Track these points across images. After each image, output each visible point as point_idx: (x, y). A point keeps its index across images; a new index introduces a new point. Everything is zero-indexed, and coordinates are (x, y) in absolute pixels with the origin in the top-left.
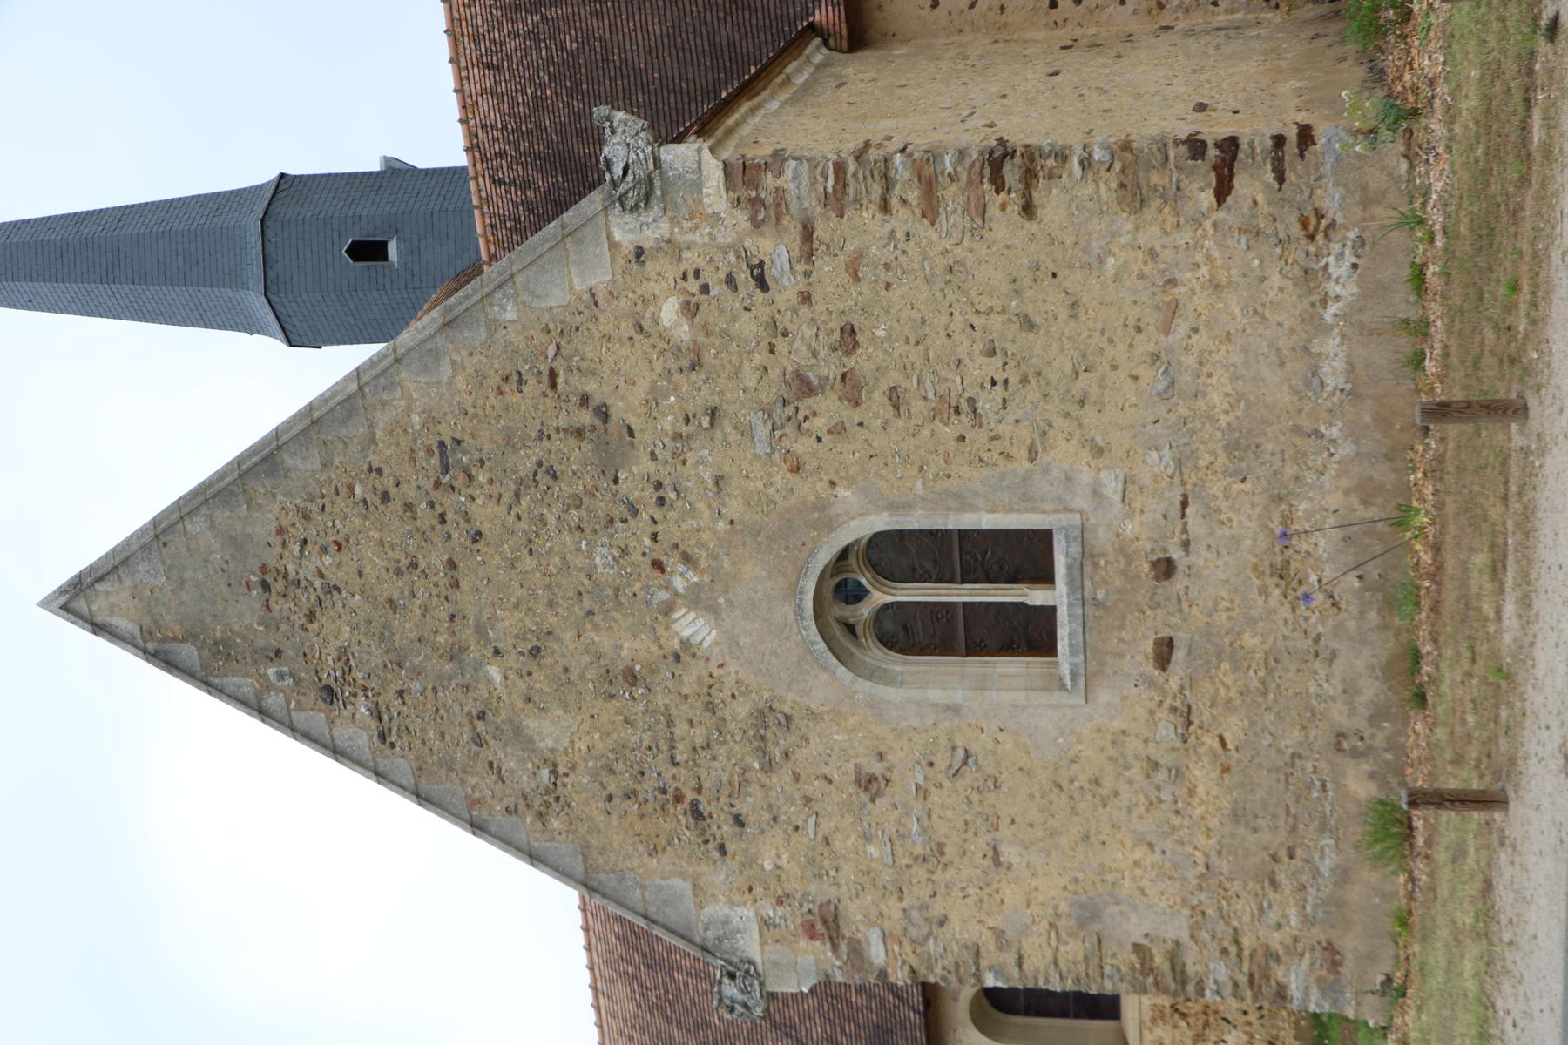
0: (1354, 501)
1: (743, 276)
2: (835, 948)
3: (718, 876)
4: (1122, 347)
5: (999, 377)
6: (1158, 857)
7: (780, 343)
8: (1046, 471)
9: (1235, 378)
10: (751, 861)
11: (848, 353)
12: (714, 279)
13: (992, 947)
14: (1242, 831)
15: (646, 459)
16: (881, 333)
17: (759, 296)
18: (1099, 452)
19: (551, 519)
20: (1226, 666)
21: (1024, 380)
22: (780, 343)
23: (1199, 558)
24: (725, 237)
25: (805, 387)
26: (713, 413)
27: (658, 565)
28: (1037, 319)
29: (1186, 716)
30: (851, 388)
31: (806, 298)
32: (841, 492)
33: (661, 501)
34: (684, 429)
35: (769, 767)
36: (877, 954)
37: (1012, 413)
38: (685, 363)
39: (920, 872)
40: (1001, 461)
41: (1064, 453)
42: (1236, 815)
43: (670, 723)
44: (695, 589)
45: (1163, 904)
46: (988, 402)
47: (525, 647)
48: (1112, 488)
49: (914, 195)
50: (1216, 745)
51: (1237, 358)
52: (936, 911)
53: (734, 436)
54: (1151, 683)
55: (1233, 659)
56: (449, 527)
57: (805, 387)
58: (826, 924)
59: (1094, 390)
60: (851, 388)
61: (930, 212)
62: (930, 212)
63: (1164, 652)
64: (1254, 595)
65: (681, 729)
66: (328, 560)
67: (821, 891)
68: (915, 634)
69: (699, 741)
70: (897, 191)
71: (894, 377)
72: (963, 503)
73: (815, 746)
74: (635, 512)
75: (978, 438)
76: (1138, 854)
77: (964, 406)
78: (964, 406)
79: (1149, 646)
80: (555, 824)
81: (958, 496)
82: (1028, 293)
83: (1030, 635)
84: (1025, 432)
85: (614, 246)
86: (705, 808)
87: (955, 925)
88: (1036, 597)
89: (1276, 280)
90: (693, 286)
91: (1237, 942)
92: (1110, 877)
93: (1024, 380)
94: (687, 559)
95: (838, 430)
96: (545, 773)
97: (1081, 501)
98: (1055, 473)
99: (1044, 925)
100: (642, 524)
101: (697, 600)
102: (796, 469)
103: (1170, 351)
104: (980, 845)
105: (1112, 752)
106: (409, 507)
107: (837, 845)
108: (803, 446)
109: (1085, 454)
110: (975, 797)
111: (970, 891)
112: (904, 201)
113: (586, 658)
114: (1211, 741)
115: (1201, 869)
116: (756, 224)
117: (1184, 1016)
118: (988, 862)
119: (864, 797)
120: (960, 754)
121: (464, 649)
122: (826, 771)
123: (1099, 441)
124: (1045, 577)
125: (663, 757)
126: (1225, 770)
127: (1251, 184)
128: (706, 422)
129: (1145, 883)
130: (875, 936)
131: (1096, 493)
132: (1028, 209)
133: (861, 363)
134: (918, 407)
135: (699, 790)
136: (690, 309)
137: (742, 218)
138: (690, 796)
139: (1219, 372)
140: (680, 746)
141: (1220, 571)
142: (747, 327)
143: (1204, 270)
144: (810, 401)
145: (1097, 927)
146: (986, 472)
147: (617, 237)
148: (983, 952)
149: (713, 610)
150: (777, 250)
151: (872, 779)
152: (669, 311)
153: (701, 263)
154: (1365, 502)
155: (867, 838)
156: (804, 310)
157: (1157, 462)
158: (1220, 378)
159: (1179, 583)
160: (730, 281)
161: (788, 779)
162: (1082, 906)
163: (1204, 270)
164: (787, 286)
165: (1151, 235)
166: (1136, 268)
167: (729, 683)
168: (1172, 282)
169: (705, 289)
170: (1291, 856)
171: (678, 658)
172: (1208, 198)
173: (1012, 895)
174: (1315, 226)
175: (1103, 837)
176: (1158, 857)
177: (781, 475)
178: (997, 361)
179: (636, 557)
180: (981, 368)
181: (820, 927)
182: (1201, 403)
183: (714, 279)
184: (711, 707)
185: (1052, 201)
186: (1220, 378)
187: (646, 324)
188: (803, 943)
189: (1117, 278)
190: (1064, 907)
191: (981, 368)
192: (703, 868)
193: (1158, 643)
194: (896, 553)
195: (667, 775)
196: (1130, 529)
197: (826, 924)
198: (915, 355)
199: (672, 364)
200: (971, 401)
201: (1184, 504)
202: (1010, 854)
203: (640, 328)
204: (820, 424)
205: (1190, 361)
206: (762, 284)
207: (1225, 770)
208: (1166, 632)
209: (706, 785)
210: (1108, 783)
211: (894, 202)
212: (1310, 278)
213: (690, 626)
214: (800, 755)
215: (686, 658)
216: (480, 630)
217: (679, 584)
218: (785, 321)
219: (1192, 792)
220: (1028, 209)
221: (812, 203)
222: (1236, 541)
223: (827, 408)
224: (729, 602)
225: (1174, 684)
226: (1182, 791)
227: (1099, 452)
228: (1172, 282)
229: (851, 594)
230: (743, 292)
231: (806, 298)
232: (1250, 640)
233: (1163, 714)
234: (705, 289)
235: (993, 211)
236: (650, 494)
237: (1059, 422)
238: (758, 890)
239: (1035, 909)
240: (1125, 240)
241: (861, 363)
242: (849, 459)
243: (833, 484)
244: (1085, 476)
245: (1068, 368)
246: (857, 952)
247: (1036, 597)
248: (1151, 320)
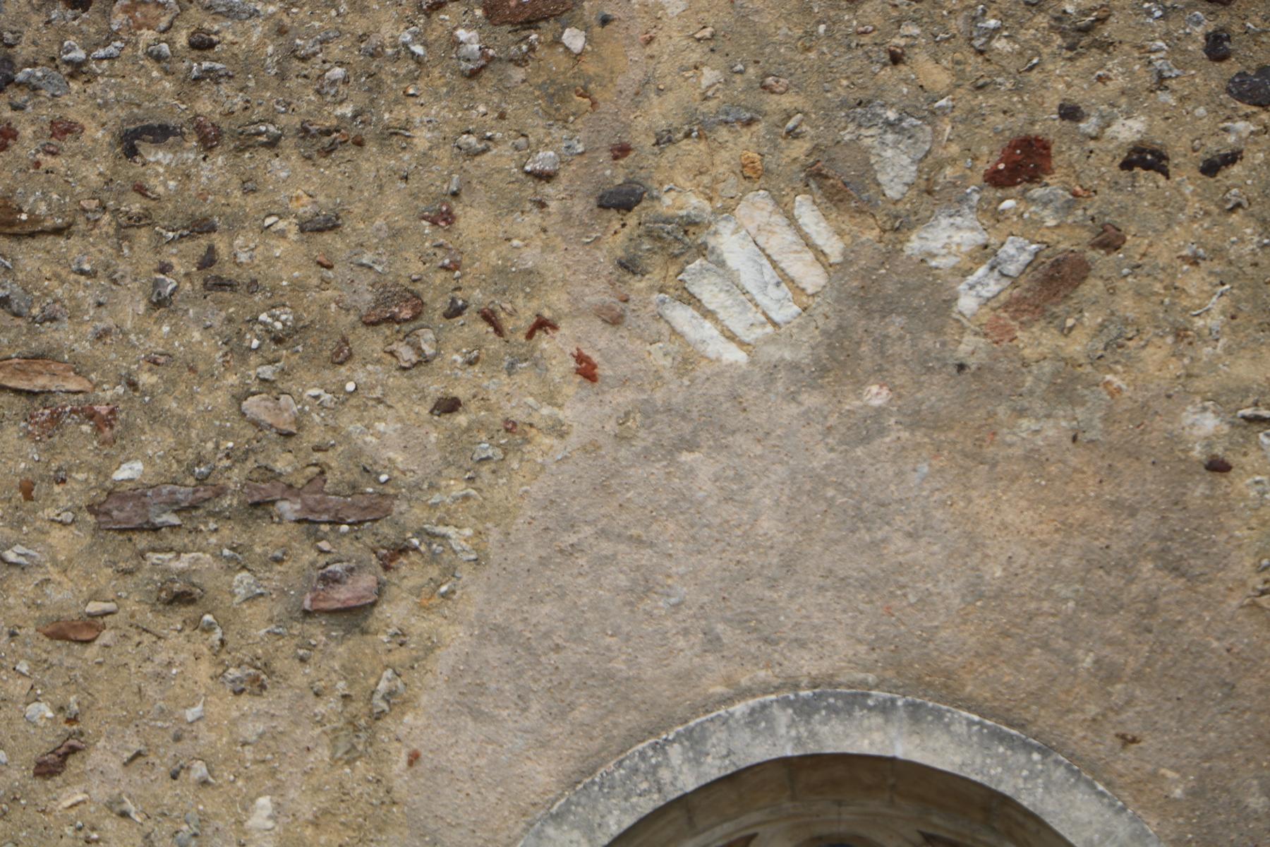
27: (1024, 163)
35: (121, 520)
43: (323, 142)
44: (929, 299)
65: (294, 181)
69: (239, 250)
94: (1056, 279)
122: (103, 756)
140: (214, 170)
149: (835, 361)
167: (513, 395)
171: (621, 200)
195: (74, 102)
214: (180, 647)
215: (618, 235)
217: (947, 238)
224: (867, 428)
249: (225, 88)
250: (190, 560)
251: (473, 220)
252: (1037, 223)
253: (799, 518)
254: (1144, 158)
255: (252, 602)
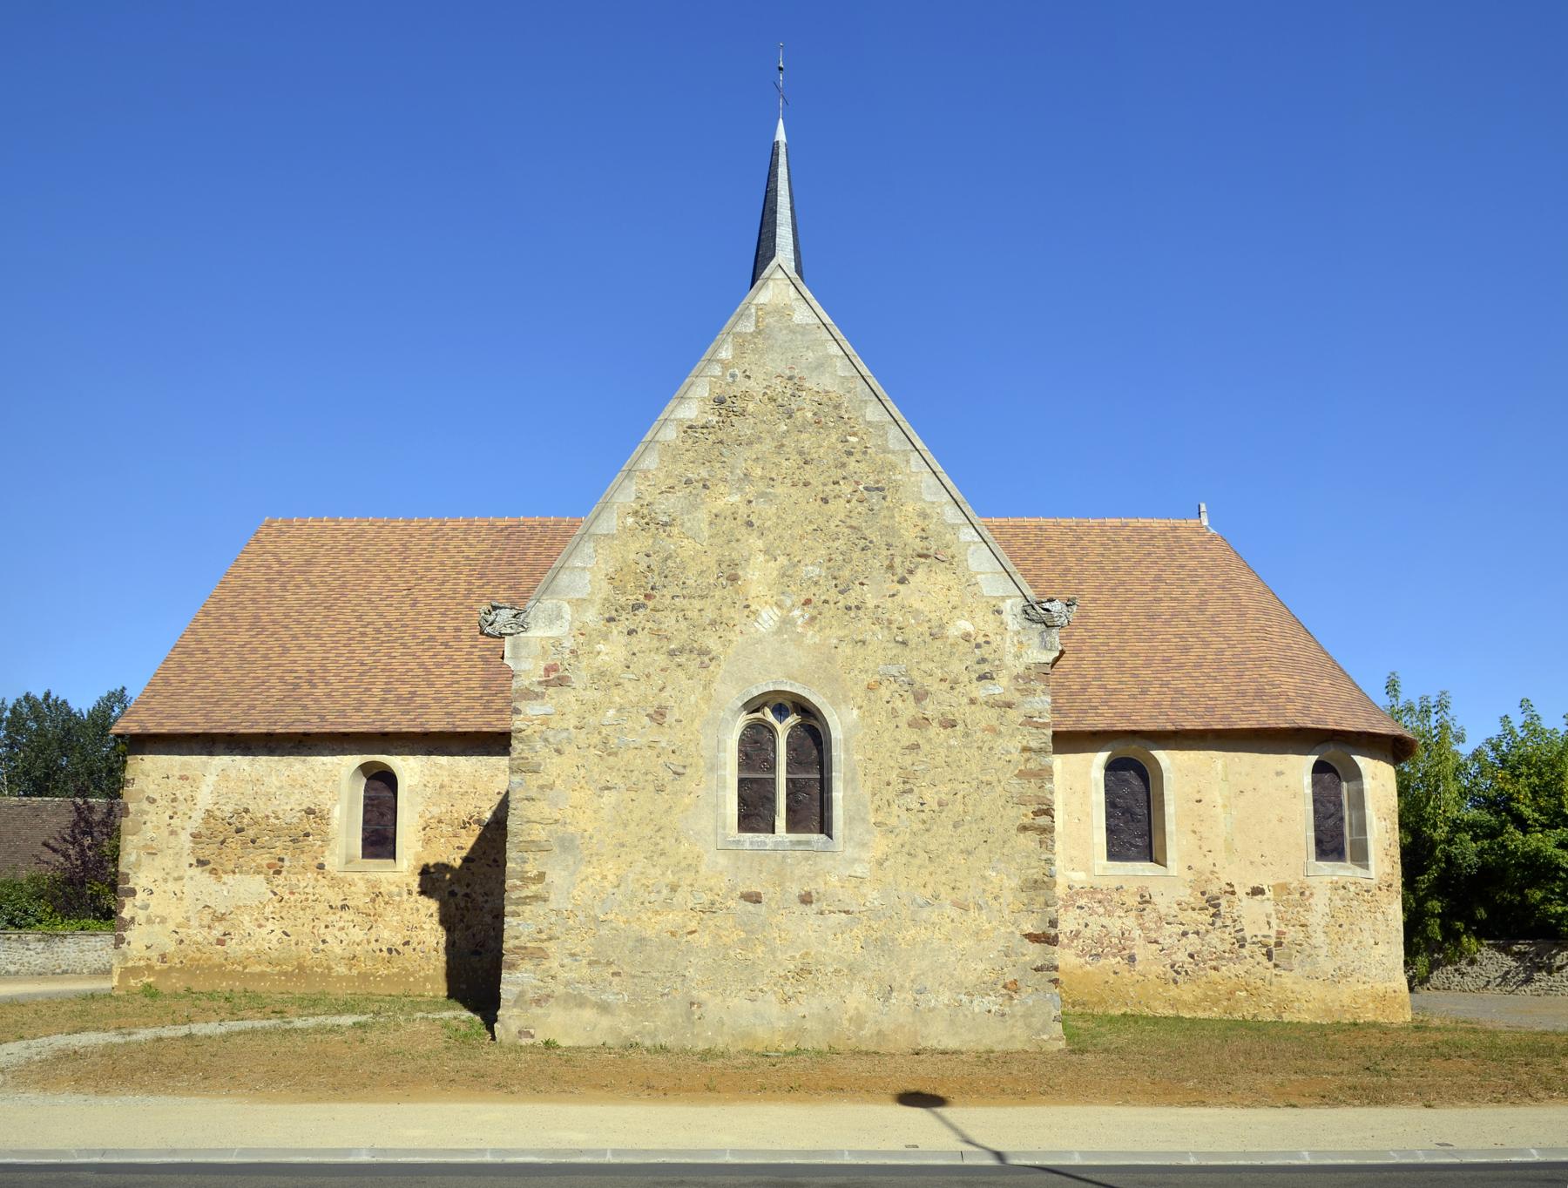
0: (852, 1012)
1: (986, 668)
2: (540, 683)
3: (591, 616)
4: (943, 879)
5: (925, 808)
6: (611, 890)
7: (946, 686)
8: (868, 832)
9: (925, 943)
10: (605, 637)
11: (941, 723)
12: (985, 651)
13: (541, 782)
14: (630, 944)
15: (875, 602)
16: (952, 742)
17: (974, 676)
18: (880, 864)
19: (836, 544)
20: (743, 935)
21: (924, 822)
22: (946, 686)
23: (813, 921)
24: (1009, 660)
25: (920, 697)
26: (904, 643)
27: (807, 602)
28: (960, 830)
29: (711, 909)
30: (920, 723)
31: (972, 702)
32: (855, 712)
33: (848, 608)
34: (894, 626)
35: (672, 653)
36: (531, 709)
37: (904, 815)
38: (935, 630)
39: (596, 739)
40: (874, 806)
41: (880, 845)
42: (642, 941)
43: (702, 597)
44: (793, 622)
45: (575, 893)
46: (911, 801)
47: (753, 518)
48: (859, 870)
49: (1032, 765)
50: (690, 929)
51: (935, 945)
52: (567, 749)
53: (890, 654)
54: (733, 890)
55: (746, 940)
56: (831, 486)
57: (920, 697)
58: (556, 679)
59: (917, 862)
60: (920, 723)
61: (1021, 774)
62: (1021, 774)
63: (754, 898)
64: (790, 953)
65: (698, 604)
66: (809, 415)
67: (580, 677)
68: (755, 746)
69: (689, 614)
70: (1033, 755)
71: (926, 747)
72: (850, 782)
73: (685, 683)
74: (841, 592)
75: (889, 793)
76: (611, 877)
77: (908, 786)
78: (908, 786)
79: (755, 889)
80: (630, 520)
81: (853, 780)
82: (974, 827)
83: (754, 813)
84: (893, 821)
85: (1003, 599)
86: (641, 612)
87: (557, 759)
88: (781, 822)
89: (981, 967)
90: (981, 640)
91: (550, 939)
92: (594, 859)
93: (924, 822)
94: (813, 619)
95: (894, 713)
96: (665, 519)
97: (850, 852)
98: (867, 837)
99: (558, 816)
100: (833, 594)
101: (786, 622)
102: (869, 688)
103: (941, 906)
104: (615, 779)
105: (683, 864)
106: (844, 465)
107: (615, 691)
108: (885, 693)
109: (879, 855)
110: (650, 777)
111: (582, 771)
112: (1028, 760)
113: (746, 553)
114: (693, 925)
115: (602, 917)
116: (1017, 677)
117: (373, 901)
118: (603, 783)
119: (650, 711)
120: (681, 770)
121: (751, 483)
122: (669, 688)
123: (887, 864)
124: (792, 826)
125: (678, 591)
126: (673, 934)
127: (1034, 952)
128: (899, 639)
129: (591, 881)
130: (549, 708)
131: (854, 861)
132: (1024, 828)
133: (934, 730)
134: (908, 760)
135: (655, 610)
136: (967, 637)
137: (1021, 670)
138: (650, 604)
139: (929, 934)
140: (685, 602)
141: (805, 932)
142: (956, 667)
143: (987, 926)
144: (912, 698)
145: (556, 850)
146: (868, 796)
147: (1009, 602)
148: (535, 776)
149: (779, 631)
150: (1000, 688)
151: (663, 715)
152: (965, 625)
153: (994, 645)
154: (850, 1020)
155: (620, 709)
156: (966, 700)
157: (872, 895)
158: (924, 935)
159: (799, 908)
160: (983, 660)
161: (663, 665)
162: (572, 841)
163: (987, 926)
164: (981, 691)
165: (1007, 897)
166: (989, 888)
167: (731, 636)
168: (980, 908)
169: (978, 646)
170: (614, 974)
171: (747, 606)
172: (1029, 929)
173: (577, 797)
174: (1013, 988)
175: (623, 856)
176: (611, 890)
177: (868, 679)
178: (936, 808)
179: (814, 589)
180: (931, 797)
181: (553, 675)
182: (909, 923)
183: (985, 651)
184: (713, 623)
185: (1029, 841)
186: (924, 935)
187: (958, 612)
188: (543, 665)
189: (983, 877)
190: (571, 829)
191: (931, 797)
192: (598, 606)
193: (758, 895)
194: (813, 736)
195: (665, 591)
196: (833, 880)
197: (556, 679)
198: (939, 760)
199: (934, 623)
200: (911, 791)
201: (847, 912)
202: (609, 798)
203: (954, 608)
204: (899, 704)
205: (934, 918)
206: (980, 678)
207: (673, 934)
208: (764, 899)
209: (658, 615)
210: (662, 860)
211: (1027, 755)
212: (984, 988)
213: (769, 617)
214: (680, 673)
215: (746, 612)
216: (763, 495)
217: (797, 613)
218: (959, 688)
219: (657, 913)
220: (1024, 828)
221: (1027, 709)
222: (825, 943)
223: (908, 709)
224: (784, 641)
225: (730, 903)
226: (656, 906)
227: (880, 864)
228: (980, 908)
229: (781, 711)
230: (977, 667)
231: (972, 702)
232: (760, 950)
233: (710, 896)
234: (978, 646)
235: (1023, 809)
236: (852, 603)
237: (899, 841)
238: (581, 639)
239: (569, 812)
240: (1006, 881)
241: (934, 730)
242: (876, 718)
243: (860, 708)
244: (866, 855)
245: (932, 847)
246: (528, 695)
247: (781, 822)
248: (959, 895)
249: (683, 625)
250: (682, 659)
251: (724, 609)
252: (810, 611)
253: (790, 355)
254: (826, 602)
255: (693, 666)
